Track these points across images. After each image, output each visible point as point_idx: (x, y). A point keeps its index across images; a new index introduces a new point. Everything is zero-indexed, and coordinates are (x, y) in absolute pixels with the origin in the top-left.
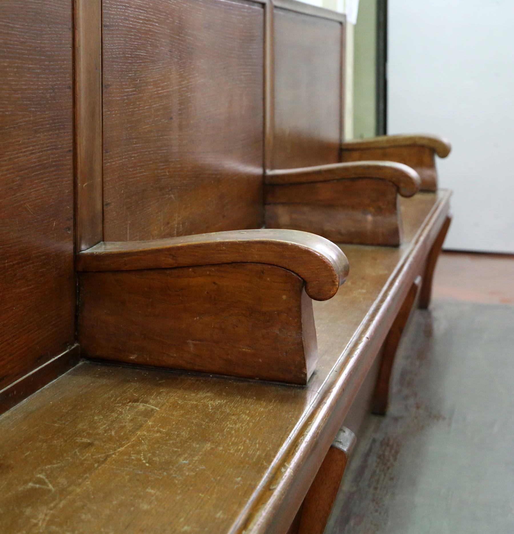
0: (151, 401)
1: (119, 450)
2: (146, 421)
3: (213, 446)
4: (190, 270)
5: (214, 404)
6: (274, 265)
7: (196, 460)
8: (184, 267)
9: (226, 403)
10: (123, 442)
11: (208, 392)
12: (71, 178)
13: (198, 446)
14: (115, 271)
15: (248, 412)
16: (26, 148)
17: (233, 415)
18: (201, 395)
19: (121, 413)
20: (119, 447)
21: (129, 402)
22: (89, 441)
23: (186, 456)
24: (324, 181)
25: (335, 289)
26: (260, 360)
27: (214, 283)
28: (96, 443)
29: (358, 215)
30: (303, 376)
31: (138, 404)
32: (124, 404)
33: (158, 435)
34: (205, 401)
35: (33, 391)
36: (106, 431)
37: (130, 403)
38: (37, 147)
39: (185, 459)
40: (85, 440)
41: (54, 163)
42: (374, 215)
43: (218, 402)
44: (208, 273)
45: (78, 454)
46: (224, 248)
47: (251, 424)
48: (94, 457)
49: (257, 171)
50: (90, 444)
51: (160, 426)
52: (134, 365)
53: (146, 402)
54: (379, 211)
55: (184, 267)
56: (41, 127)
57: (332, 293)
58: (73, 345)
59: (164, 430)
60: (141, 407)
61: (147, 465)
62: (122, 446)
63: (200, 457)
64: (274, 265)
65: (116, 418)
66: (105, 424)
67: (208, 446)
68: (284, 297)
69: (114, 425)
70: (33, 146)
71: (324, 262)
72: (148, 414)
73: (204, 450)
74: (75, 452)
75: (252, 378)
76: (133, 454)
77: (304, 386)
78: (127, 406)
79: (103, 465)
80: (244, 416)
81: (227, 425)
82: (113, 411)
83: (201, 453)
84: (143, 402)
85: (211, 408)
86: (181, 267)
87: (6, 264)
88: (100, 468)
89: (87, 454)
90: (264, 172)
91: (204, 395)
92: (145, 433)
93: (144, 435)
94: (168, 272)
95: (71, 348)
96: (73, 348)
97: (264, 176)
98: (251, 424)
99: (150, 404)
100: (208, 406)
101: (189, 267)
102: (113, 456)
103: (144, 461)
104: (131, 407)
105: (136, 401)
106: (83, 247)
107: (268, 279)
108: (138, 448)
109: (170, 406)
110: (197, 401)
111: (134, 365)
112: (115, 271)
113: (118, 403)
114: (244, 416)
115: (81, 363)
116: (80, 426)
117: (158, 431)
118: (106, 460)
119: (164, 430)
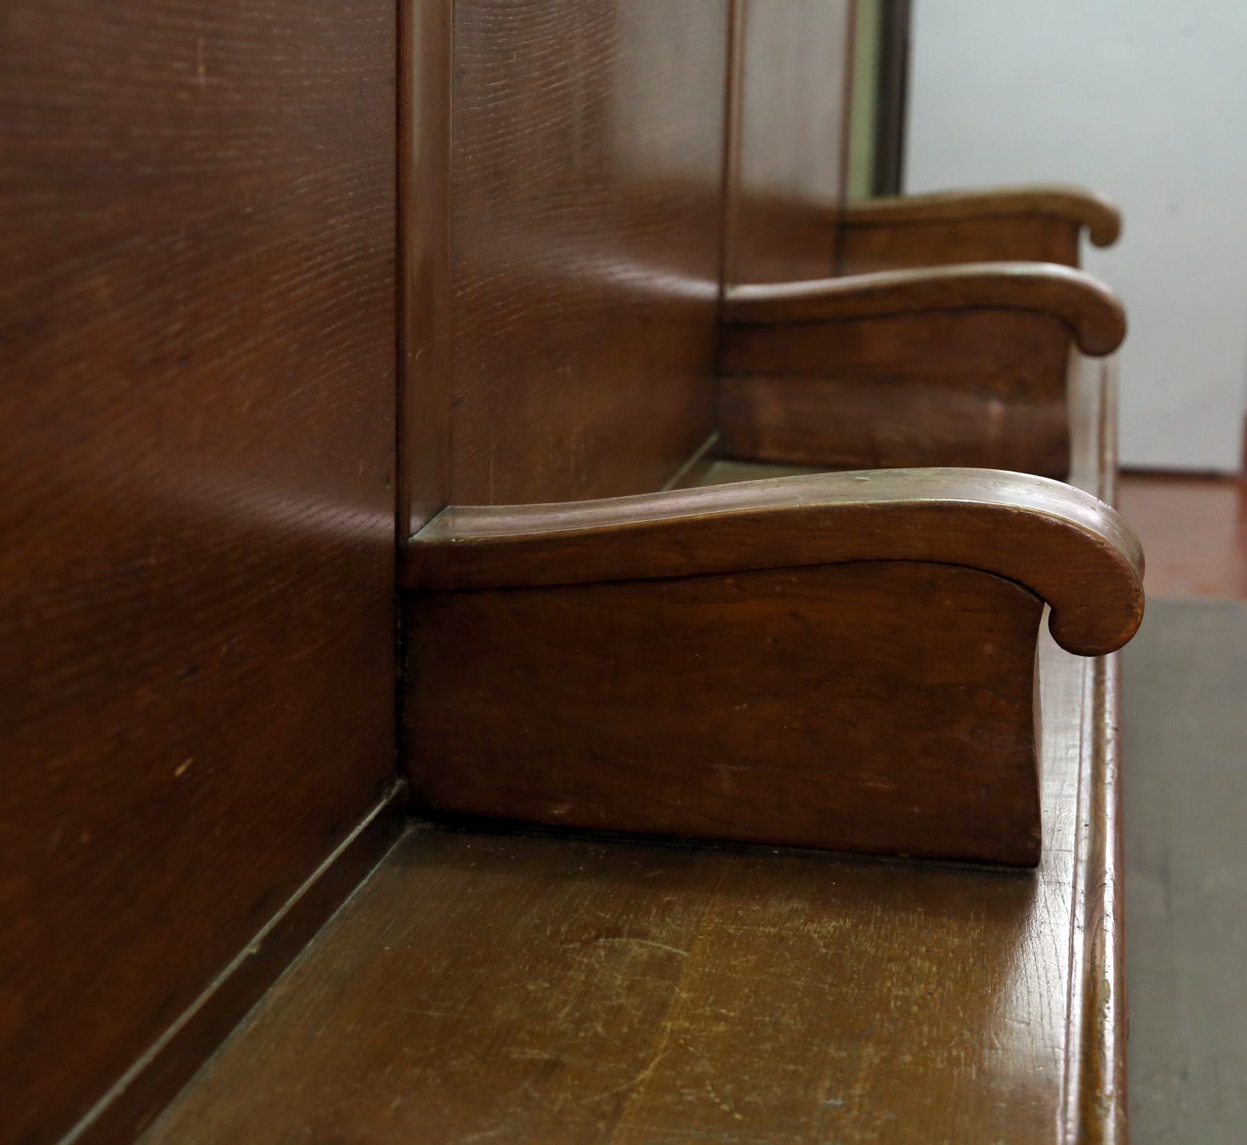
0: (654, 931)
1: (640, 1077)
2: (670, 989)
3: (885, 1054)
4: (729, 581)
5: (824, 932)
6: (966, 566)
7: (861, 1097)
8: (711, 575)
9: (854, 926)
10: (641, 1055)
11: (790, 897)
12: (392, 338)
13: (843, 1054)
14: (508, 589)
15: (924, 949)
16: (309, 259)
17: (890, 960)
18: (778, 907)
19: (592, 972)
20: (638, 1071)
21: (598, 937)
22: (546, 1056)
23: (828, 1084)
24: (884, 316)
25: (1132, 626)
26: (916, 810)
27: (795, 615)
28: (567, 1058)
29: (966, 402)
30: (1031, 845)
31: (624, 940)
32: (586, 944)
33: (721, 1027)
34: (797, 923)
35: (324, 918)
36: (578, 1024)
37: (602, 940)
38: (330, 255)
39: (830, 1093)
40: (533, 1053)
41: (361, 299)
42: (1007, 400)
43: (831, 926)
44: (778, 589)
45: (536, 1095)
46: (828, 523)
47: (949, 984)
48: (584, 1102)
49: (704, 289)
50: (552, 1067)
51: (715, 1003)
52: (561, 831)
53: (643, 934)
54: (1020, 391)
55: (711, 575)
56: (336, 198)
57: (1124, 636)
58: (392, 784)
59: (732, 1014)
60: (637, 949)
61: (738, 1116)
62: (643, 1065)
63: (867, 1086)
64: (966, 566)
65: (585, 983)
66: (565, 1004)
67: (870, 1053)
68: (988, 648)
69: (592, 1007)
70: (323, 253)
71: (1108, 557)
72: (665, 968)
73: (865, 1065)
74: (526, 1091)
75: (891, 853)
76: (683, 1087)
77: (1029, 870)
78: (596, 947)
79: (620, 1125)
80: (919, 962)
81: (889, 990)
82: (568, 966)
83: (861, 1074)
84: (633, 934)
85: (821, 943)
86: (703, 575)
87: (273, 590)
88: (615, 1133)
89: (562, 1096)
90: (722, 292)
91: (785, 909)
92: (686, 1025)
93: (687, 1031)
94: (665, 588)
95: (390, 792)
96: (394, 791)
97: (721, 303)
98: (949, 984)
99: (654, 939)
100: (811, 939)
101: (726, 574)
102: (634, 1096)
103: (725, 1107)
104: (611, 950)
105: (615, 932)
106: (415, 522)
107: (948, 602)
108: (688, 1068)
109: (713, 944)
110: (774, 925)
111: (561, 831)
112: (508, 589)
113: (571, 942)
114: (919, 962)
115: (409, 831)
116: (499, 1012)
117: (717, 1018)
118: (618, 1109)
119: (732, 1014)
